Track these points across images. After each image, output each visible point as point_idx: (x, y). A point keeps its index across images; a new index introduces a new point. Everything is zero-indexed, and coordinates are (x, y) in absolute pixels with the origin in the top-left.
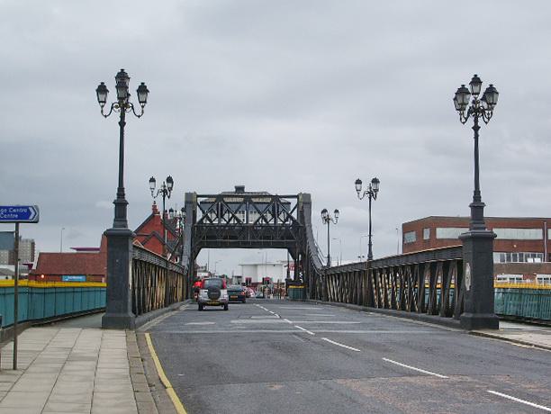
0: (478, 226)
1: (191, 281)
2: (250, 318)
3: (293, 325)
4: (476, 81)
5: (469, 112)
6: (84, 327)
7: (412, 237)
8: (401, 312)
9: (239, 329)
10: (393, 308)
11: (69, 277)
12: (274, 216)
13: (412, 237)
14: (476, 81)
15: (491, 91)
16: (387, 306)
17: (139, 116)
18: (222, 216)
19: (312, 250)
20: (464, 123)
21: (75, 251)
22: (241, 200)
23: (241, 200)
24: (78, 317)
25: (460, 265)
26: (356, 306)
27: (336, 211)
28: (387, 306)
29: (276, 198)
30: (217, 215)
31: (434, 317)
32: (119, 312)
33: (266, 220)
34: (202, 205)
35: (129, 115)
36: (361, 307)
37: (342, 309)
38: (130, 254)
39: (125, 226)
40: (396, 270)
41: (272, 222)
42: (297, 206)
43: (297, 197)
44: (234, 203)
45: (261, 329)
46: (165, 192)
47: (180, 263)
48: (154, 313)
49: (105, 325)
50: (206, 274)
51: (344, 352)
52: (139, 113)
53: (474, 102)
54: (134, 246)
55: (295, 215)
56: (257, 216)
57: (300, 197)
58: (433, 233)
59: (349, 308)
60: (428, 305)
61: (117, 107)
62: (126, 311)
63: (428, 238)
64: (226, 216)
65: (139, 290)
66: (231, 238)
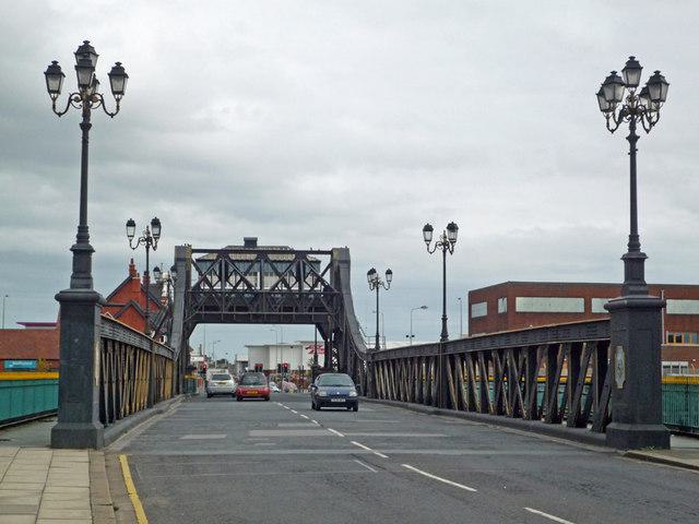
0: (635, 289)
1: (185, 376)
2: (276, 428)
3: (347, 439)
4: (633, 66)
5: (623, 114)
6: (24, 444)
7: (481, 310)
8: (512, 420)
9: (267, 448)
10: (471, 410)
11: (14, 363)
12: (298, 279)
13: (481, 310)
14: (633, 66)
15: (657, 81)
16: (473, 408)
17: (112, 115)
18: (227, 279)
19: (352, 326)
20: (612, 131)
21: (24, 327)
22: (253, 257)
23: (253, 257)
24: (19, 424)
25: (602, 348)
26: (422, 407)
27: (389, 272)
28: (473, 408)
29: (302, 254)
30: (220, 279)
31: (533, 423)
32: (80, 421)
33: (287, 285)
34: (199, 264)
35: (96, 113)
36: (431, 409)
37: (448, 419)
38: (97, 330)
39: (89, 286)
40: (487, 355)
41: (296, 288)
42: (330, 266)
43: (330, 253)
44: (241, 261)
45: (299, 447)
46: (149, 241)
47: (168, 343)
48: (134, 418)
49: (58, 441)
50: (202, 359)
51: (452, 491)
52: (111, 109)
53: (631, 99)
54: (103, 318)
55: (327, 278)
56: (275, 279)
57: (335, 254)
58: (511, 305)
59: (411, 409)
60: (541, 408)
61: (77, 100)
62: (89, 419)
63: (500, 301)
64: (232, 279)
65: (110, 382)
66: (239, 309)
